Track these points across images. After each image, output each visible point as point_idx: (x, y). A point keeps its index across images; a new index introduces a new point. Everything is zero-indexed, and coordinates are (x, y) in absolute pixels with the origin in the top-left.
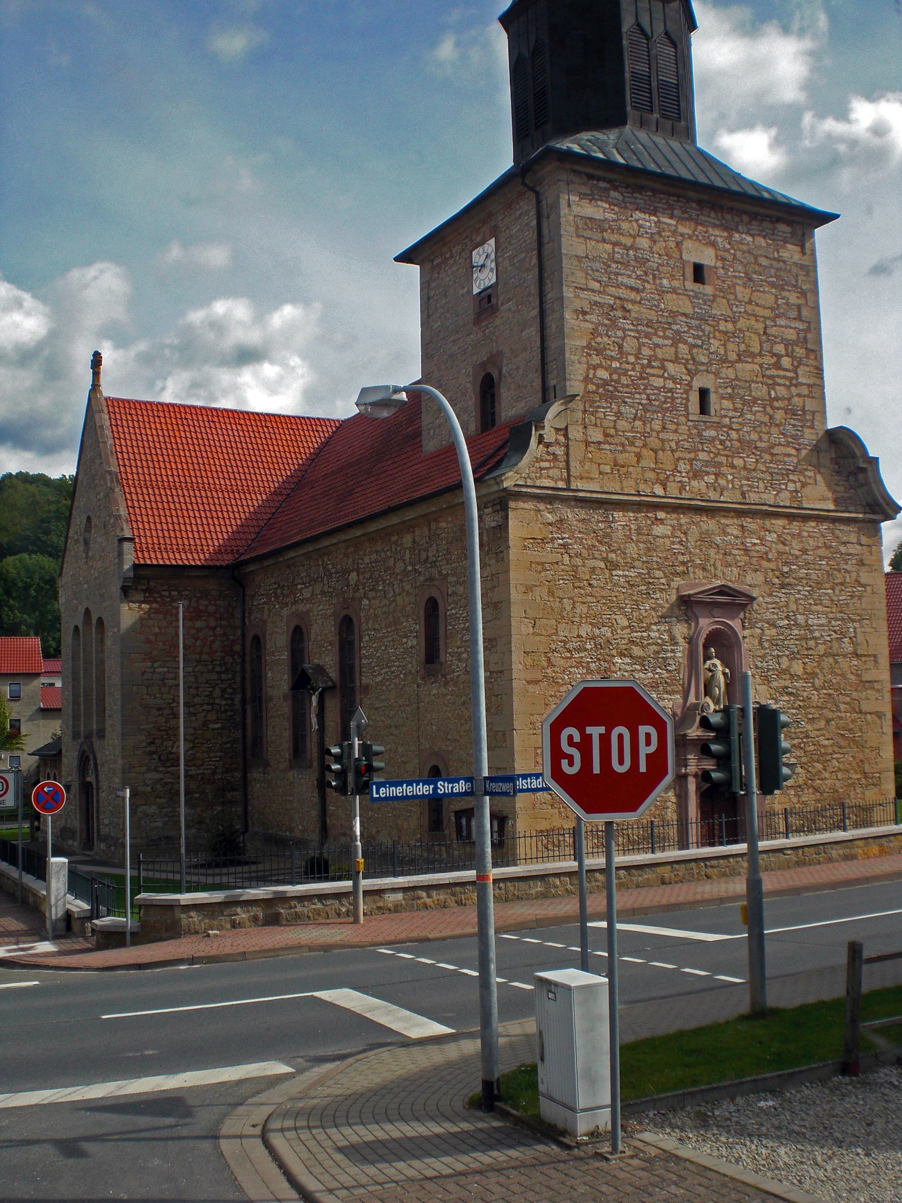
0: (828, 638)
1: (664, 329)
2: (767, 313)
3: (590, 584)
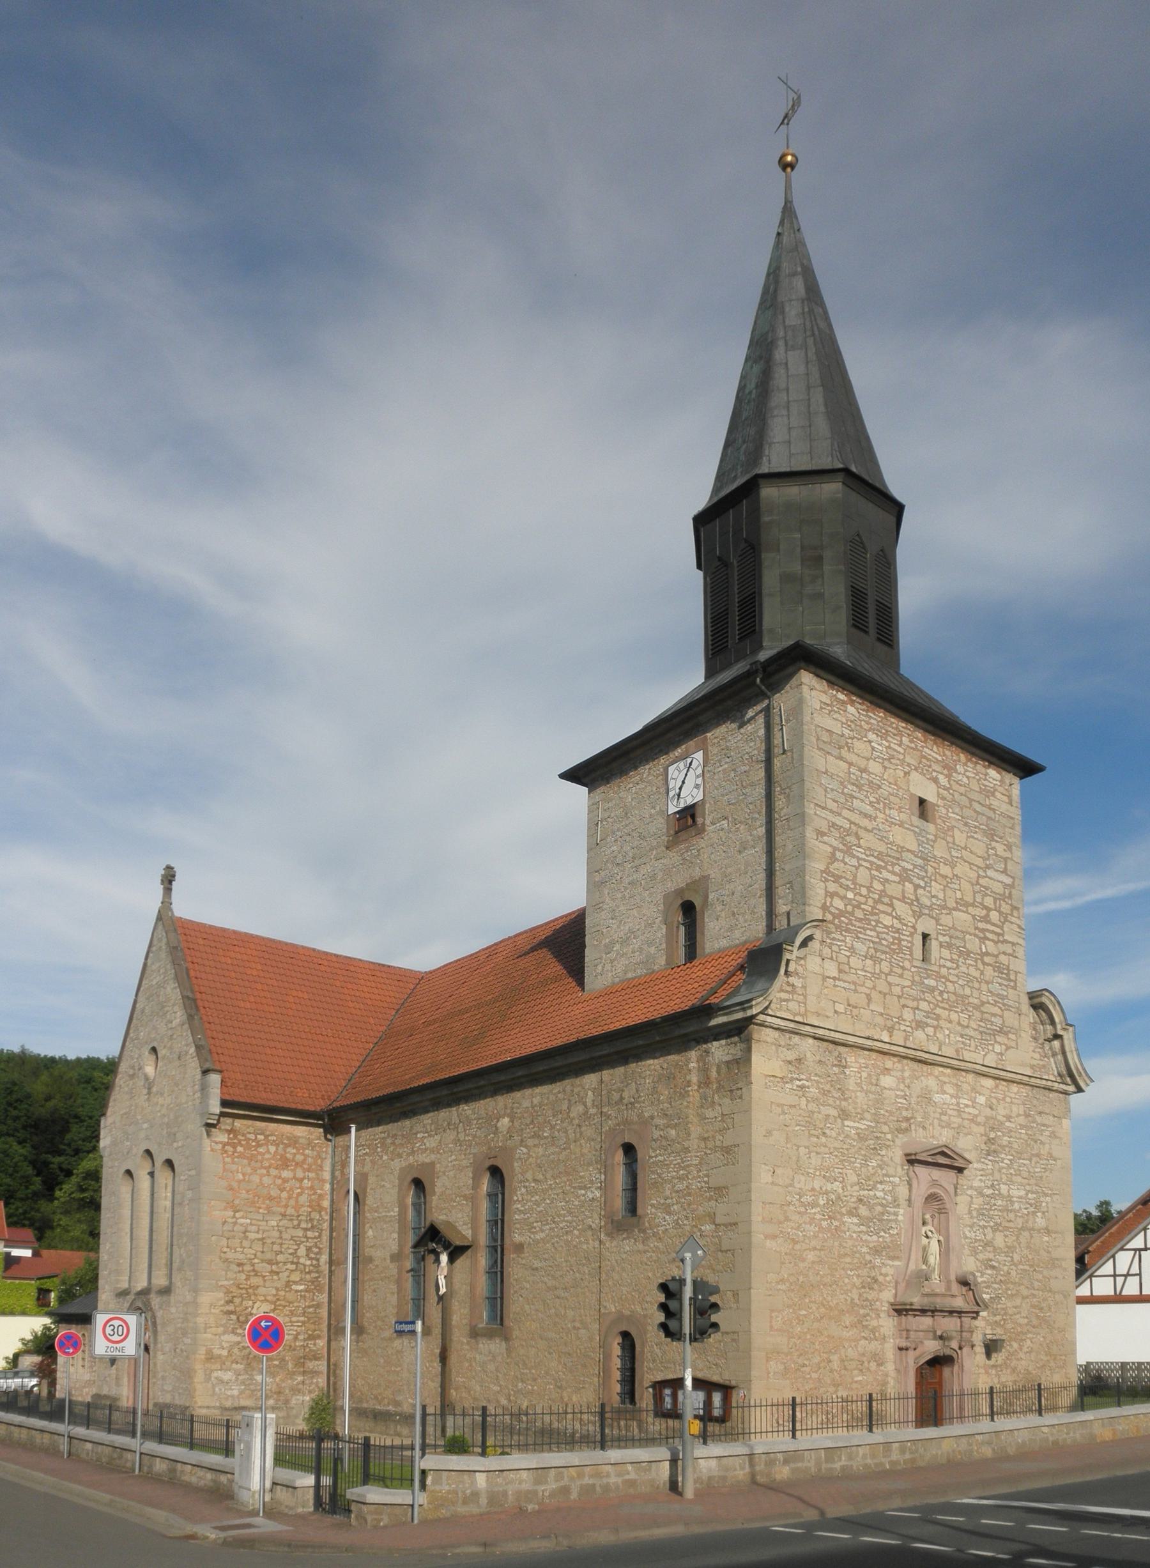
0: (1026, 1212)
1: (893, 864)
2: (979, 862)
3: (824, 1133)
